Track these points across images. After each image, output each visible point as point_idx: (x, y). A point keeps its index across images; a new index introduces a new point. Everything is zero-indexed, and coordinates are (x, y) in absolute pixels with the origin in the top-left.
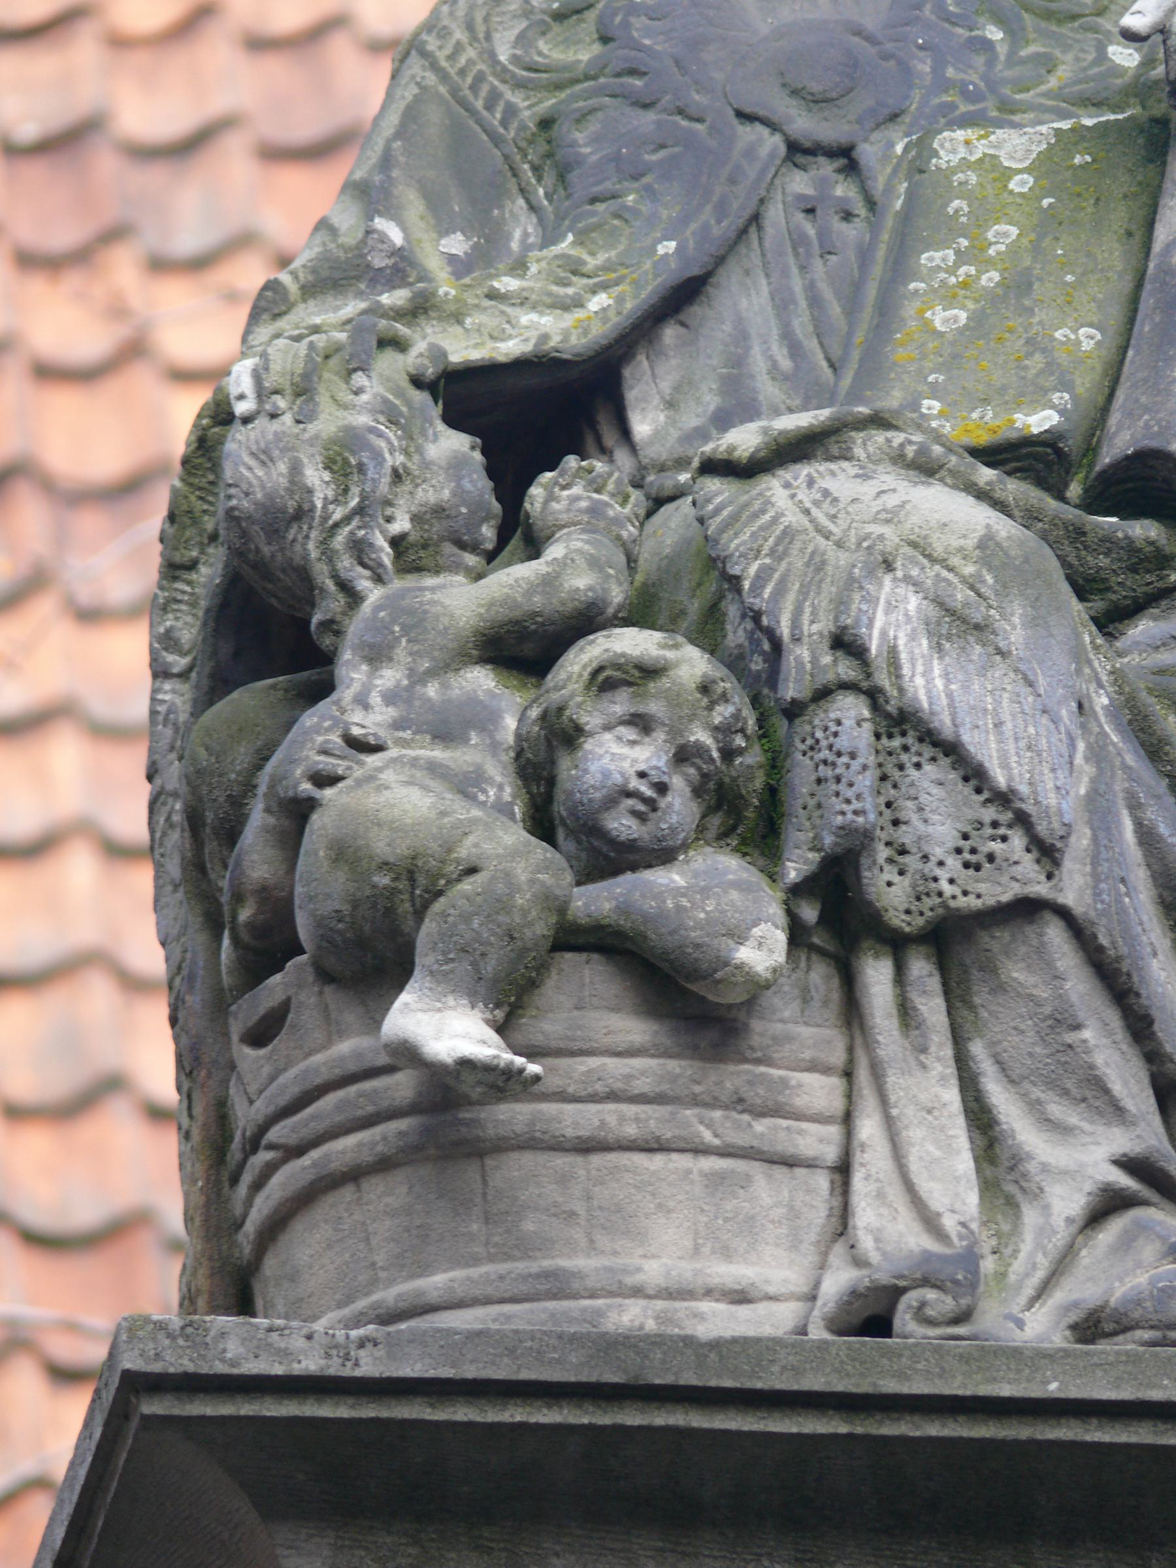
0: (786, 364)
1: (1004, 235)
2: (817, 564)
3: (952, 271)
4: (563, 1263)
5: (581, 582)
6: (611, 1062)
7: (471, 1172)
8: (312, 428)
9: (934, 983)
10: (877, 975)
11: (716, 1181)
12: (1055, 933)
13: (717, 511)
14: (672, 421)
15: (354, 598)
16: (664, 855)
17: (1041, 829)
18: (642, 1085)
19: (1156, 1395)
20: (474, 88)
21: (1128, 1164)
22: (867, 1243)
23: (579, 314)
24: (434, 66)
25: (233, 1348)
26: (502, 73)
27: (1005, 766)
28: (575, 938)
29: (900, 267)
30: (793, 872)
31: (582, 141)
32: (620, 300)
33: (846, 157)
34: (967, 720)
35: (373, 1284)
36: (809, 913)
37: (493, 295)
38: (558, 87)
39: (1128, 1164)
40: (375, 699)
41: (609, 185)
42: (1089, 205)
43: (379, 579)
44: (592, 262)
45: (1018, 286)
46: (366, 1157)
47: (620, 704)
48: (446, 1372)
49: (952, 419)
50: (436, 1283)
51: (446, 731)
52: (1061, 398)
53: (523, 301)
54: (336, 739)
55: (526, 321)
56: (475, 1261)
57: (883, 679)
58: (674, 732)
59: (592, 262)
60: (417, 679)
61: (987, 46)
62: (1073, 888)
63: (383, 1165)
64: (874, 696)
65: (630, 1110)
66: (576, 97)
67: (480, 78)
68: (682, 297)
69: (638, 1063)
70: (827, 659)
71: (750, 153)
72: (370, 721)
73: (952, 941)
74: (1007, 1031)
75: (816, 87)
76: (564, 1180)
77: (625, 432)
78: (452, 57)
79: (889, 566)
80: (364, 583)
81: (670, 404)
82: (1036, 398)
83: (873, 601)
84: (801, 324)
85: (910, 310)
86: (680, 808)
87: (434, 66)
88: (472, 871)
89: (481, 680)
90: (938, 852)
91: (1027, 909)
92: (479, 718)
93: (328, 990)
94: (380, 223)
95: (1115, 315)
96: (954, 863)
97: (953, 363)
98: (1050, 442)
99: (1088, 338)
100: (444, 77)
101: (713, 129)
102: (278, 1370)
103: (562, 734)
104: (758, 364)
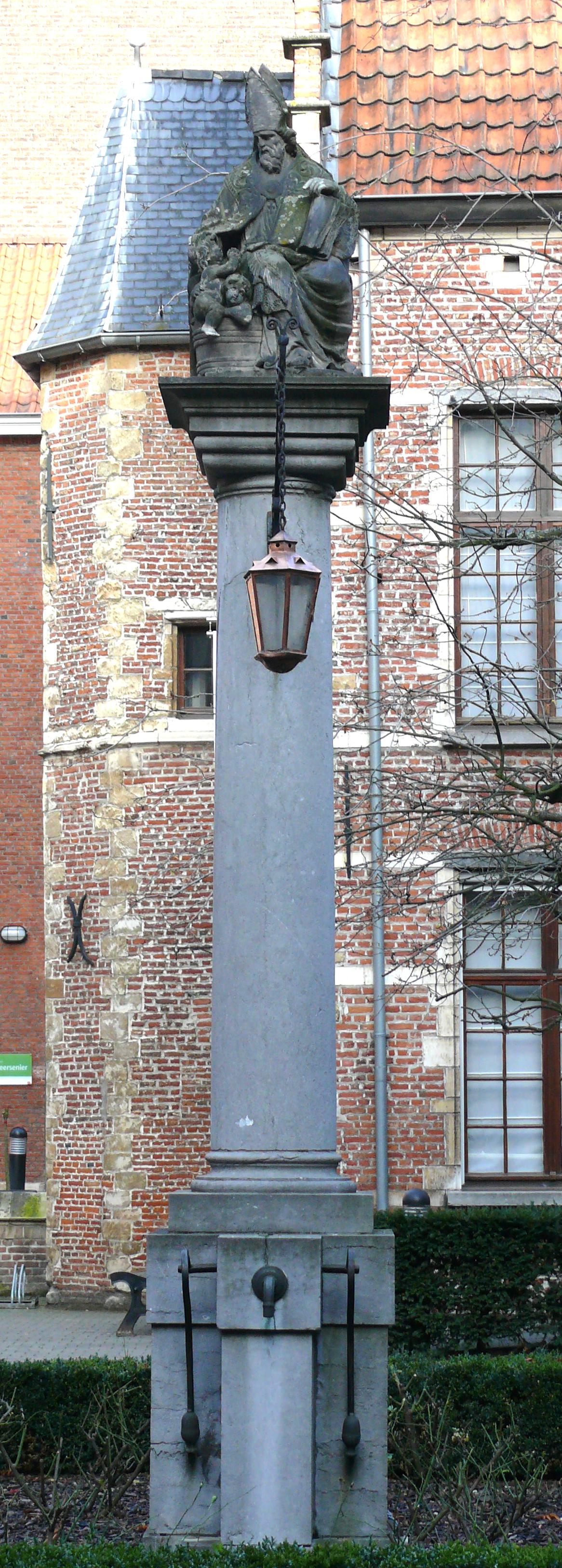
1: (291, 213)
5: (230, 268)
16: (238, 304)
28: (225, 316)
29: (278, 218)
31: (243, 197)
33: (274, 200)
45: (292, 221)
50: (211, 359)
51: (212, 288)
55: (231, 225)
62: (289, 308)
68: (252, 220)
72: (202, 287)
82: (291, 238)
86: (240, 298)
89: (218, 280)
91: (282, 311)
92: (216, 286)
99: (300, 228)
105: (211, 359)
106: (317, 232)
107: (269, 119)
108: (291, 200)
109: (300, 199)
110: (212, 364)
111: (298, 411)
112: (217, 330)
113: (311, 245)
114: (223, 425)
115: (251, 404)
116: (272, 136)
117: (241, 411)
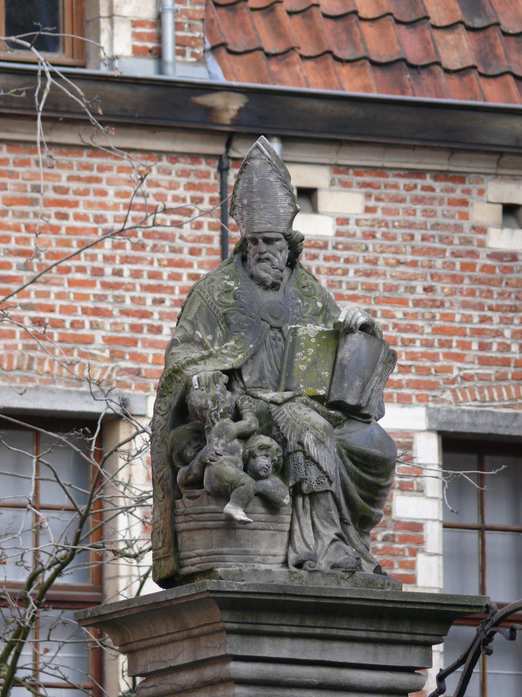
0: (270, 369)
1: (311, 351)
2: (294, 426)
3: (302, 357)
4: (248, 549)
6: (258, 515)
7: (233, 532)
8: (210, 394)
9: (309, 502)
10: (300, 500)
11: (272, 535)
12: (330, 495)
13: (274, 411)
14: (251, 378)
15: (214, 424)
16: (266, 478)
17: (331, 479)
18: (263, 519)
19: (363, 597)
20: (211, 305)
21: (337, 535)
22: (298, 549)
23: (237, 359)
24: (203, 299)
25: (225, 586)
26: (216, 303)
27: (326, 467)
30: (291, 484)
31: (232, 319)
32: (244, 356)
33: (280, 329)
34: (320, 459)
35: (212, 547)
36: (291, 490)
37: (222, 353)
38: (227, 307)
39: (337, 535)
40: (219, 445)
41: (238, 329)
42: (325, 347)
43: (218, 420)
44: (239, 347)
45: (314, 362)
46: (214, 526)
47: (264, 452)
48: (256, 591)
49: (306, 390)
50: (225, 550)
52: (325, 388)
53: (227, 355)
54: (214, 453)
56: (232, 547)
57: (306, 450)
58: (272, 457)
59: (239, 347)
60: (227, 442)
61: (298, 304)
63: (217, 528)
64: (304, 453)
65: (260, 523)
66: (230, 310)
67: (212, 303)
69: (262, 515)
70: (297, 445)
71: (264, 327)
72: (219, 449)
73: (313, 496)
74: (320, 510)
75: (276, 316)
76: (248, 535)
77: (242, 379)
78: (207, 298)
79: (308, 430)
80: (216, 421)
81: (250, 375)
83: (305, 436)
84: (273, 361)
85: (296, 365)
87: (203, 299)
88: (243, 485)
89: (236, 442)
90: (313, 481)
91: (326, 491)
93: (209, 497)
94: (197, 332)
95: (331, 370)
96: (315, 483)
97: (304, 377)
98: (323, 396)
100: (205, 302)
101: (257, 321)
102: (231, 590)
103: (253, 455)
104: (266, 369)
105: (225, 550)
106: (358, 383)
107: (278, 216)
108: (311, 330)
109: (322, 333)
110: (228, 557)
111: (363, 634)
112: (247, 513)
113: (351, 401)
114: (268, 648)
115: (308, 622)
116: (278, 239)
117: (294, 630)
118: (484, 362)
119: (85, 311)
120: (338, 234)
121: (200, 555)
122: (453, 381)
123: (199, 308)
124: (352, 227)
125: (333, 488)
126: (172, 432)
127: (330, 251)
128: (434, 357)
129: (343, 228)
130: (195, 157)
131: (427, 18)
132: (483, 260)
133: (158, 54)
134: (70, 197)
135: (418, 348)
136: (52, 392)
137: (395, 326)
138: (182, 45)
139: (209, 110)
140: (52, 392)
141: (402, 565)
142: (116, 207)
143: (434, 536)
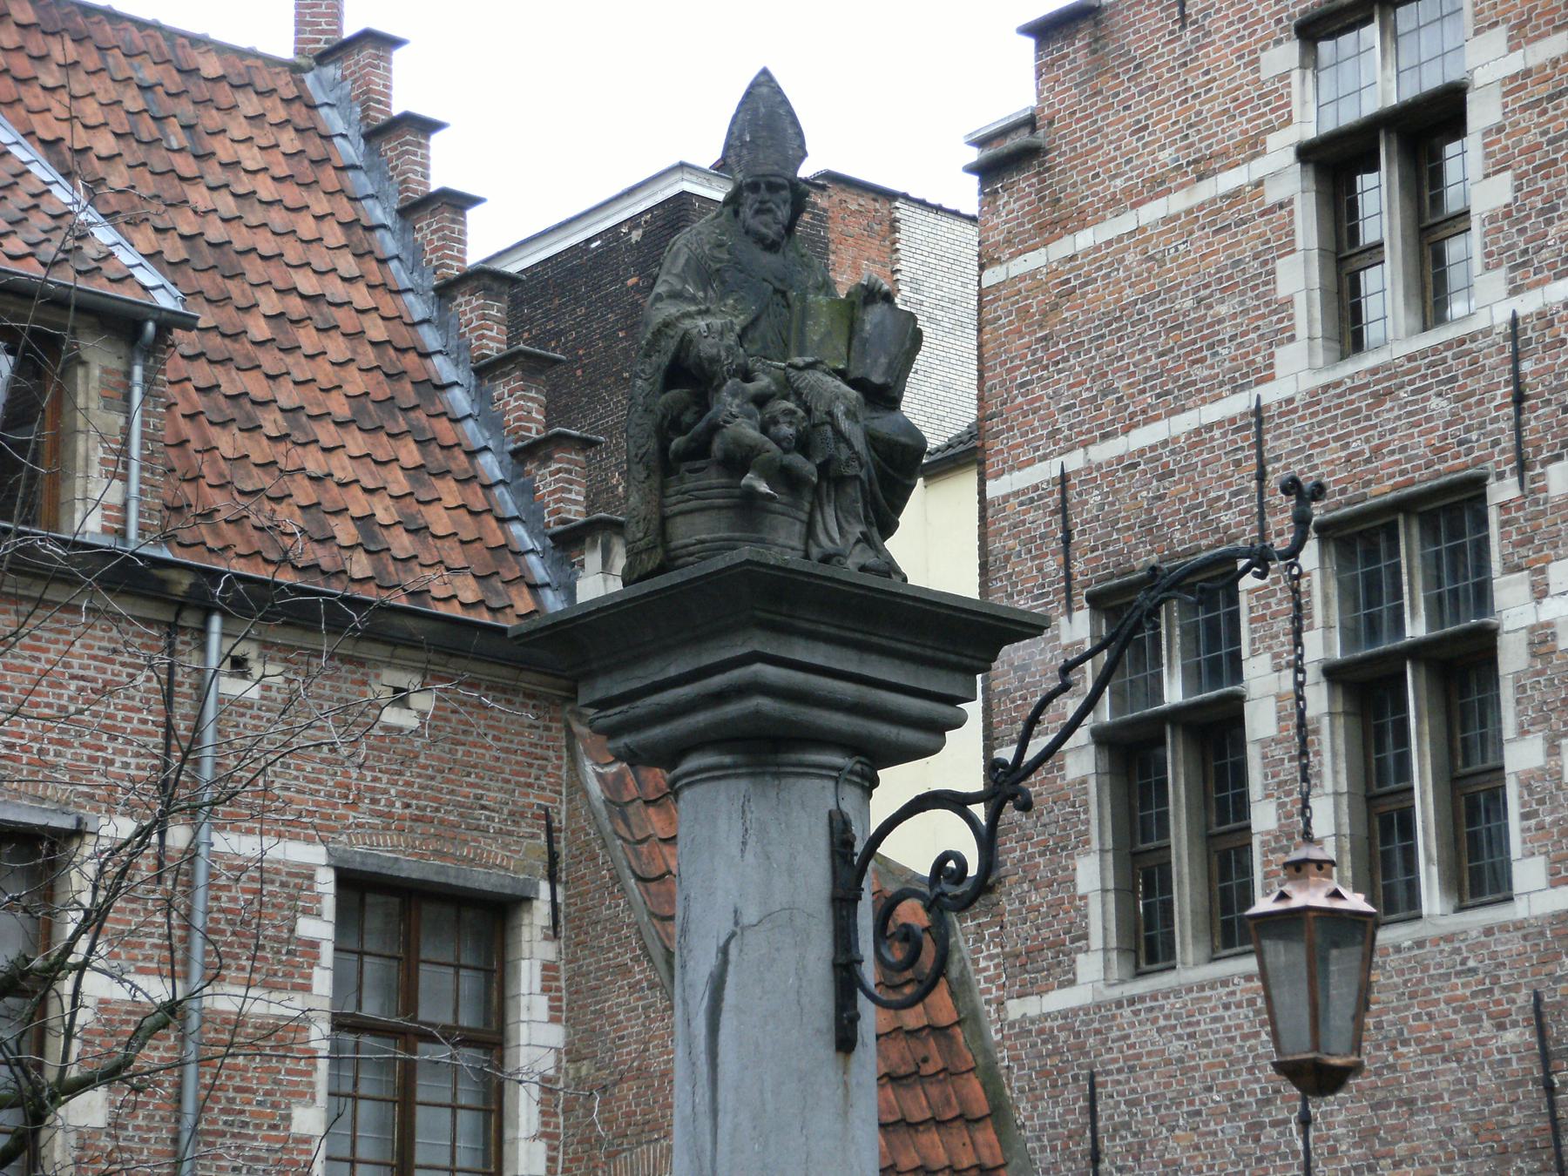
118: (374, 813)
119: (50, 741)
120: (263, 698)
121: (702, 542)
122: (349, 827)
123: (687, 261)
124: (274, 694)
125: (863, 474)
126: (663, 397)
127: (255, 712)
128: (334, 806)
129: (266, 694)
130: (149, 623)
131: (334, 537)
132: (376, 731)
133: (122, 534)
134: (43, 644)
135: (321, 798)
136: (19, 806)
137: (305, 778)
138: (143, 529)
139: (163, 582)
140: (19, 806)
141: (302, 976)
142: (81, 656)
143: (327, 952)
